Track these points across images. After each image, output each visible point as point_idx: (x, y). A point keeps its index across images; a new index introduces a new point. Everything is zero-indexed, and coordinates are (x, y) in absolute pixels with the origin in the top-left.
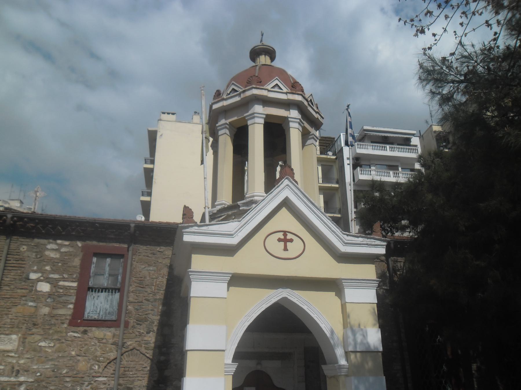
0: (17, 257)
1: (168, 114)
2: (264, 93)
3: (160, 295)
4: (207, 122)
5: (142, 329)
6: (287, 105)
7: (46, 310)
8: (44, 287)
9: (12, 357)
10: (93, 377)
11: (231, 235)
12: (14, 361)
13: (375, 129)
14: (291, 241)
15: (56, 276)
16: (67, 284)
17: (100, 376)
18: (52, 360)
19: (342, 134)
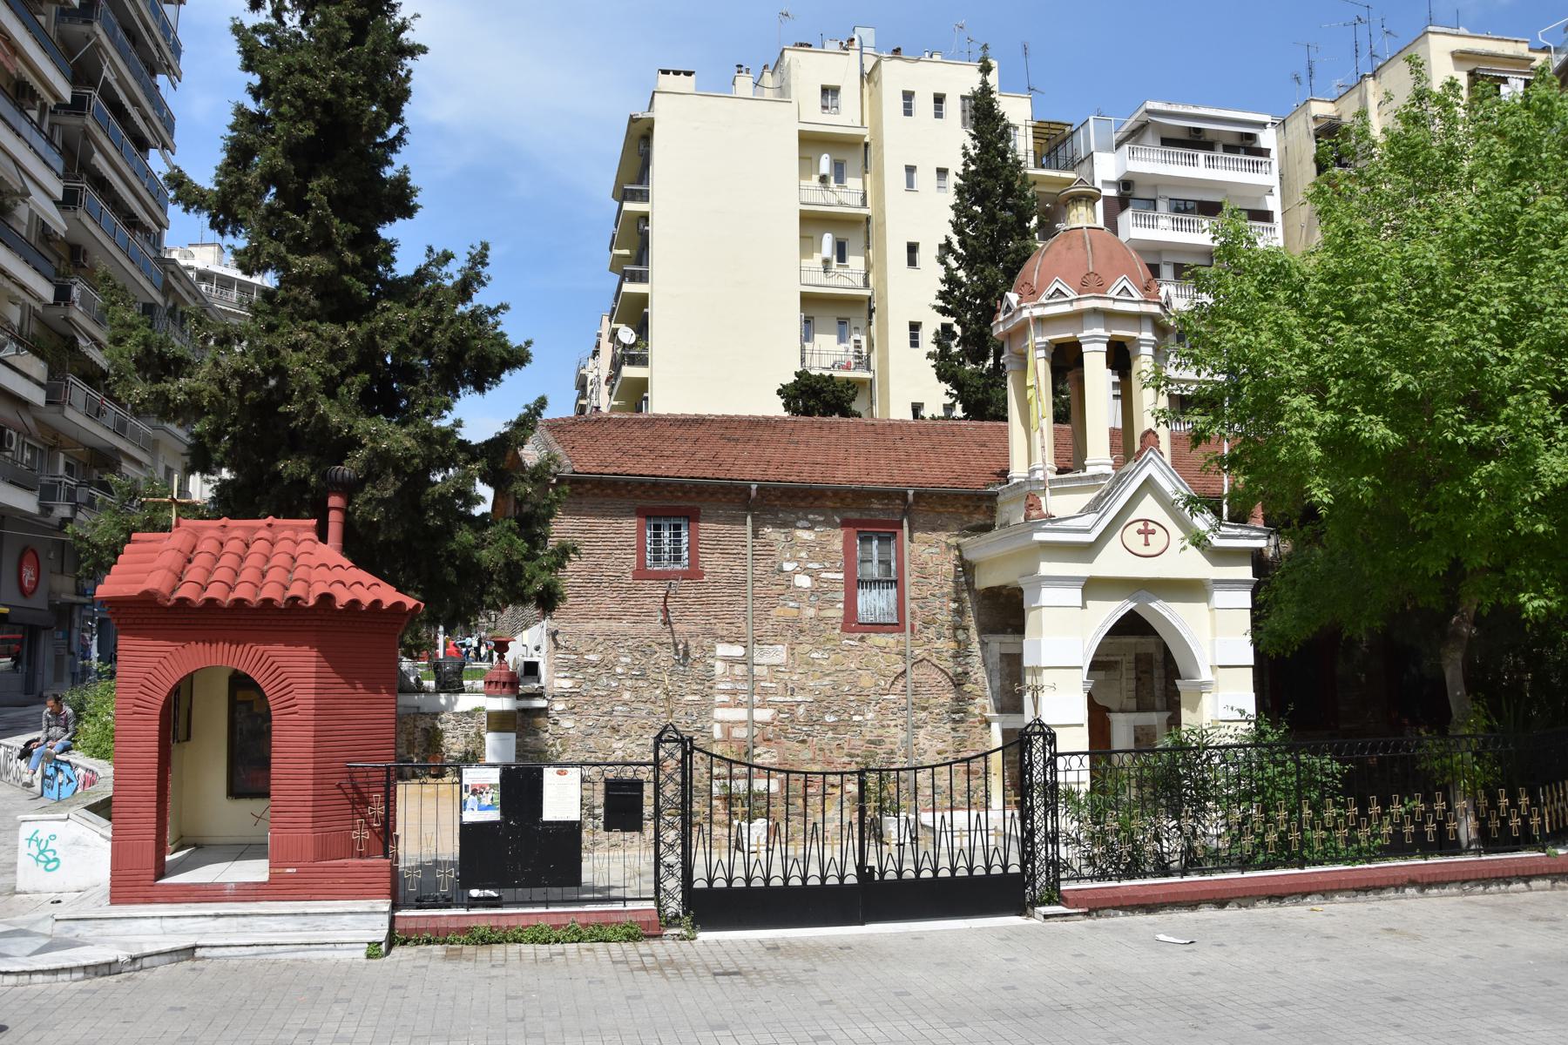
1: (677, 73)
2: (1108, 305)
3: (948, 588)
6: (1138, 318)
7: (811, 612)
8: (803, 581)
11: (1087, 531)
13: (1180, 109)
14: (1153, 532)
15: (816, 566)
16: (830, 576)
18: (828, 675)
19: (1091, 119)
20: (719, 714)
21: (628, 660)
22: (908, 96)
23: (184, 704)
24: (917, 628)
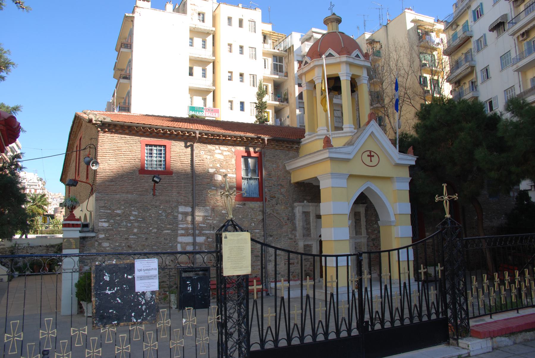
0: (200, 158)
4: (337, 93)
5: (274, 202)
9: (209, 219)
10: (252, 229)
11: (349, 154)
12: (211, 222)
14: (373, 156)
17: (256, 229)
20: (180, 239)
21: (136, 213)
22: (230, 19)
23: (515, 70)
24: (268, 199)
